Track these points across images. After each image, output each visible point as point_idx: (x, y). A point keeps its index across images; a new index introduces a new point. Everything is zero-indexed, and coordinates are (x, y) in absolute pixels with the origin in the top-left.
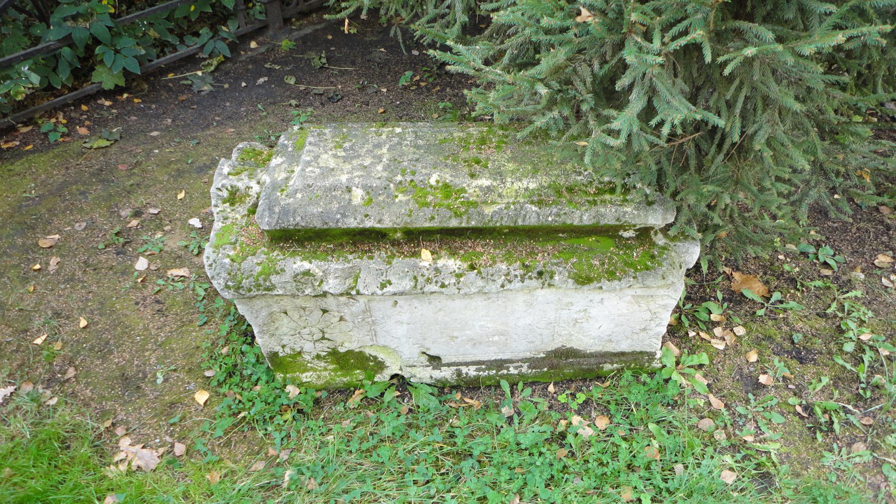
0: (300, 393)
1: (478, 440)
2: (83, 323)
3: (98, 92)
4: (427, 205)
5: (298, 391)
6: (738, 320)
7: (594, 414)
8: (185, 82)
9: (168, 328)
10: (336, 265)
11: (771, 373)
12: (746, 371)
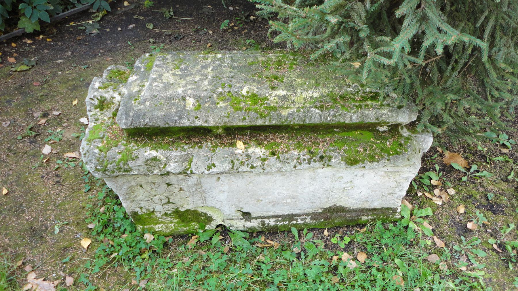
0: (154, 239)
1: (278, 272)
2: (5, 191)
3: (23, 34)
4: (241, 109)
5: (153, 237)
6: (449, 184)
7: (356, 251)
8: (81, 28)
9: (63, 194)
10: (175, 153)
11: (474, 221)
12: (457, 220)
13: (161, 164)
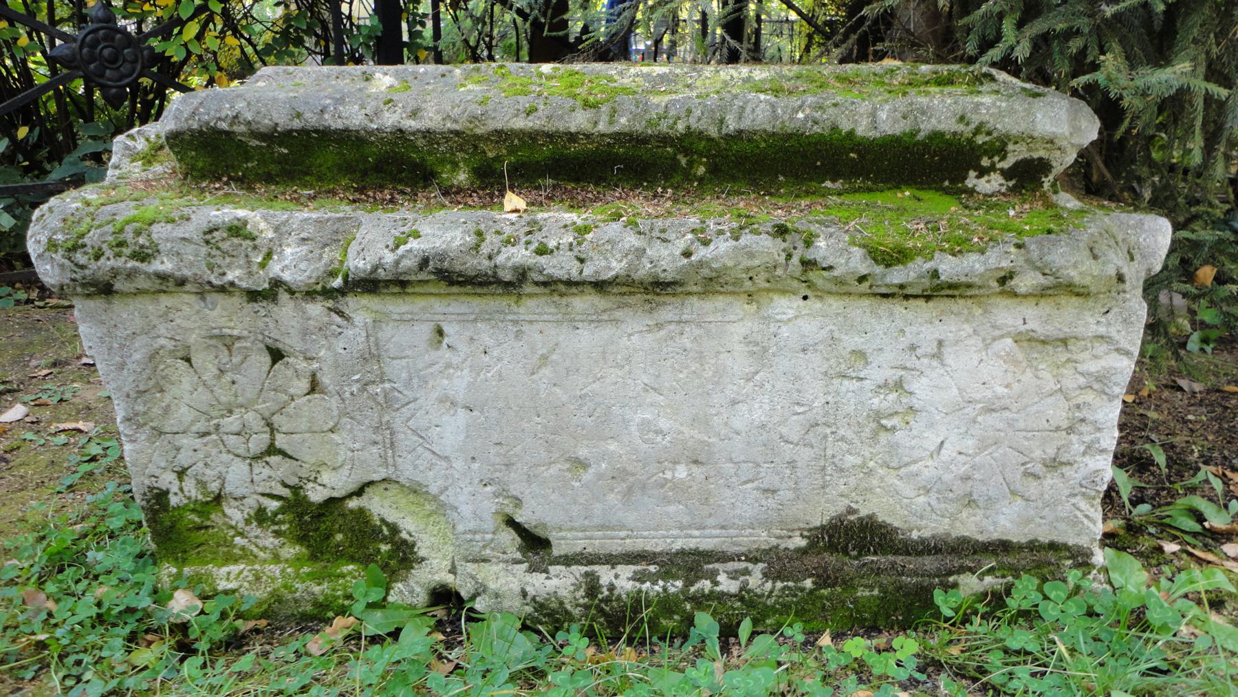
13: (255, 247)
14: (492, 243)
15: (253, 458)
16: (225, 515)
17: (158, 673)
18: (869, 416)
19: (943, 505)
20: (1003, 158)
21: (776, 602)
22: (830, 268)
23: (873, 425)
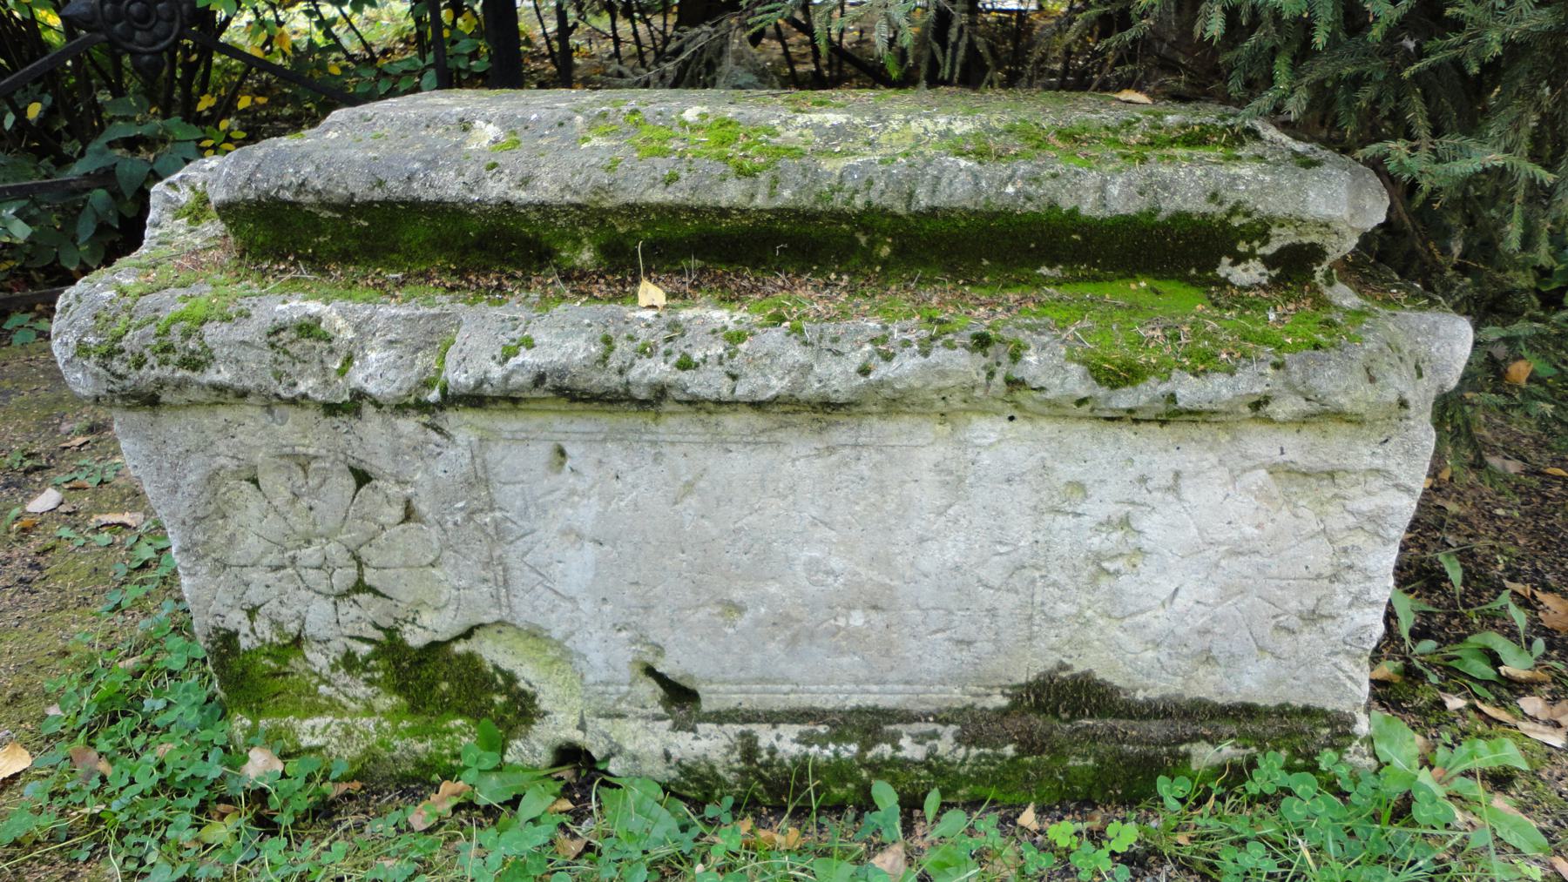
13: (331, 351)
14: (623, 353)
15: (337, 596)
16: (306, 660)
17: (235, 857)
18: (1087, 558)
19: (1175, 662)
20: (1265, 243)
21: (971, 770)
22: (1042, 389)
23: (1092, 568)
